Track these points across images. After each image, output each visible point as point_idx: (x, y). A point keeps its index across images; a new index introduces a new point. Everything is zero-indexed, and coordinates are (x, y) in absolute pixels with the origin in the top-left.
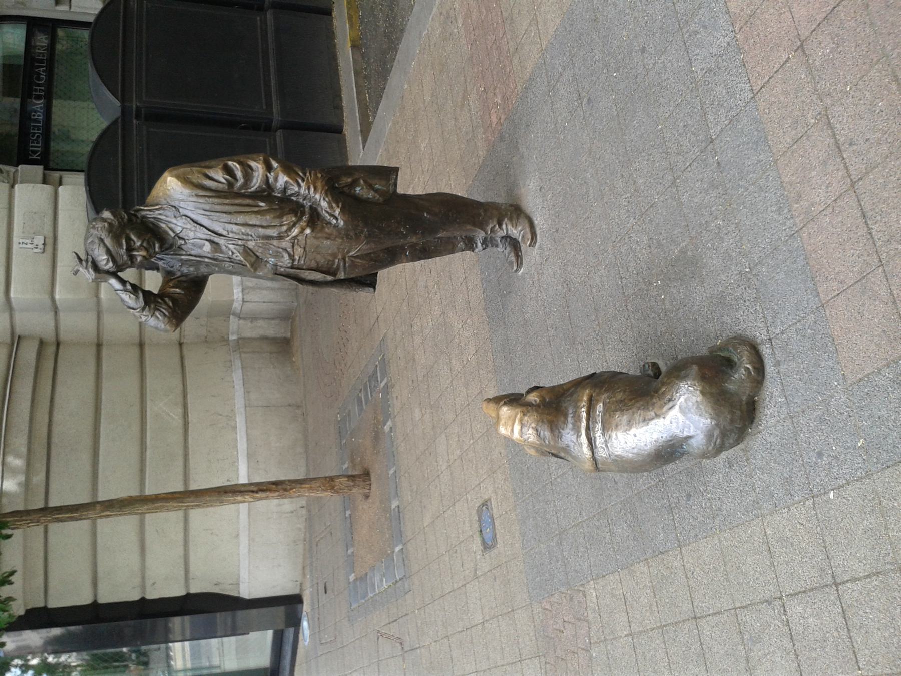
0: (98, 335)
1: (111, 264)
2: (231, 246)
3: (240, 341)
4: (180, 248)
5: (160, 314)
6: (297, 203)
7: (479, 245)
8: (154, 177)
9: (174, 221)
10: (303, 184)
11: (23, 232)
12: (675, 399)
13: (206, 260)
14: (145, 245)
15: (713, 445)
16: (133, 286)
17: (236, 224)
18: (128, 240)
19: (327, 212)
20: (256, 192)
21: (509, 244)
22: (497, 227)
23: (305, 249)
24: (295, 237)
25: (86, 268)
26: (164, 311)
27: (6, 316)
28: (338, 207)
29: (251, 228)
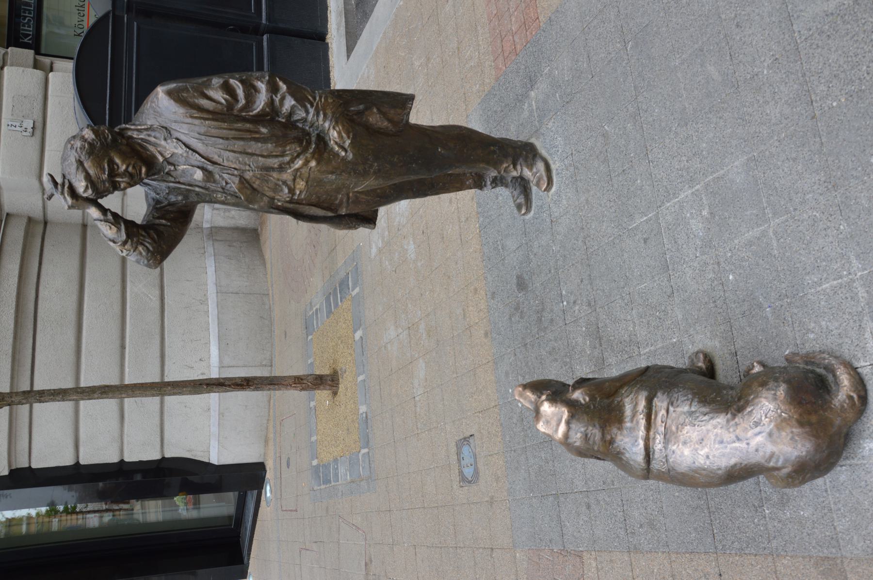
0: (83, 219)
1: (90, 191)
2: (225, 176)
3: (213, 229)
4: (168, 174)
5: (143, 249)
6: (303, 130)
7: (489, 183)
8: (144, 92)
9: (163, 143)
11: (12, 115)
13: (197, 189)
14: (130, 169)
16: (115, 215)
18: (111, 163)
19: (336, 143)
20: (258, 115)
21: (520, 184)
22: (512, 166)
23: (307, 182)
24: (298, 170)
26: (148, 245)
28: (349, 137)
29: (249, 156)
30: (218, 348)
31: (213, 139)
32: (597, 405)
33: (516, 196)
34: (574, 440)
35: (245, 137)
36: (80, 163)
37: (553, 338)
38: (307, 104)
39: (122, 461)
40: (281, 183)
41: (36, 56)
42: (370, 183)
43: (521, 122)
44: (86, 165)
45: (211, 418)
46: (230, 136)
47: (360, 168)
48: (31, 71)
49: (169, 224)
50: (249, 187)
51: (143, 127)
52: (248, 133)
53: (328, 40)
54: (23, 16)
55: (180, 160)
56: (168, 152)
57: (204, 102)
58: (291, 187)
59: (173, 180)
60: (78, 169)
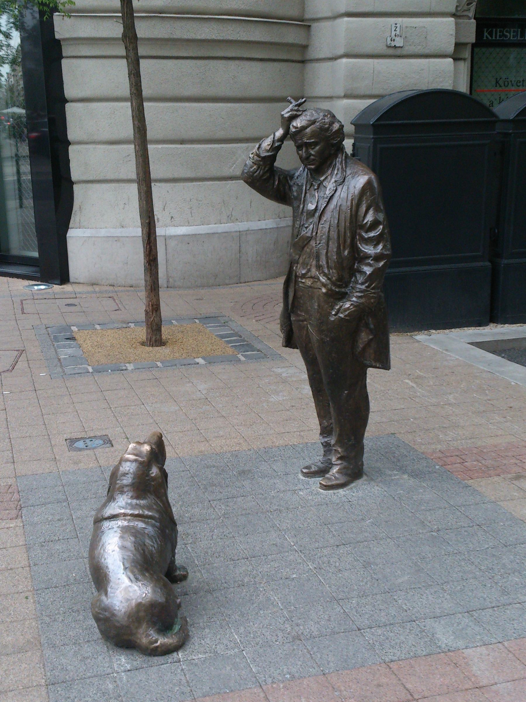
1: (294, 130)
2: (312, 226)
4: (312, 185)
6: (350, 282)
7: (326, 440)
9: (333, 180)
10: (363, 287)
11: (407, 27)
12: (137, 582)
13: (301, 206)
14: (312, 157)
15: (99, 611)
17: (329, 232)
18: (315, 144)
19: (341, 307)
20: (358, 248)
22: (339, 456)
23: (310, 287)
24: (319, 279)
25: (292, 110)
26: (258, 172)
27: (329, 14)
28: (345, 316)
30: (184, 234)
31: (337, 216)
32: (149, 482)
33: (317, 464)
34: (124, 466)
35: (340, 239)
36: (314, 122)
37: (198, 494)
38: (368, 283)
39: (68, 143)
40: (309, 267)
41: (471, 45)
42: (315, 336)
43: (382, 469)
44: (312, 126)
45: (115, 229)
46: (340, 228)
47: (324, 328)
48: (453, 42)
49: (275, 187)
50: (304, 244)
51: (343, 165)
52: (343, 241)
53: (492, 325)
54: (510, 31)
55: (322, 193)
56: (327, 184)
57: (363, 208)
58: (306, 275)
59: (308, 188)
60: (310, 121)
